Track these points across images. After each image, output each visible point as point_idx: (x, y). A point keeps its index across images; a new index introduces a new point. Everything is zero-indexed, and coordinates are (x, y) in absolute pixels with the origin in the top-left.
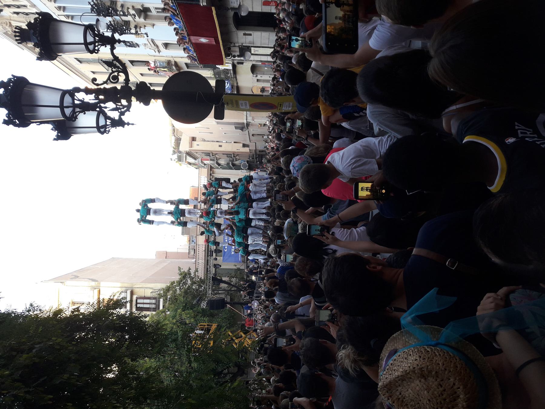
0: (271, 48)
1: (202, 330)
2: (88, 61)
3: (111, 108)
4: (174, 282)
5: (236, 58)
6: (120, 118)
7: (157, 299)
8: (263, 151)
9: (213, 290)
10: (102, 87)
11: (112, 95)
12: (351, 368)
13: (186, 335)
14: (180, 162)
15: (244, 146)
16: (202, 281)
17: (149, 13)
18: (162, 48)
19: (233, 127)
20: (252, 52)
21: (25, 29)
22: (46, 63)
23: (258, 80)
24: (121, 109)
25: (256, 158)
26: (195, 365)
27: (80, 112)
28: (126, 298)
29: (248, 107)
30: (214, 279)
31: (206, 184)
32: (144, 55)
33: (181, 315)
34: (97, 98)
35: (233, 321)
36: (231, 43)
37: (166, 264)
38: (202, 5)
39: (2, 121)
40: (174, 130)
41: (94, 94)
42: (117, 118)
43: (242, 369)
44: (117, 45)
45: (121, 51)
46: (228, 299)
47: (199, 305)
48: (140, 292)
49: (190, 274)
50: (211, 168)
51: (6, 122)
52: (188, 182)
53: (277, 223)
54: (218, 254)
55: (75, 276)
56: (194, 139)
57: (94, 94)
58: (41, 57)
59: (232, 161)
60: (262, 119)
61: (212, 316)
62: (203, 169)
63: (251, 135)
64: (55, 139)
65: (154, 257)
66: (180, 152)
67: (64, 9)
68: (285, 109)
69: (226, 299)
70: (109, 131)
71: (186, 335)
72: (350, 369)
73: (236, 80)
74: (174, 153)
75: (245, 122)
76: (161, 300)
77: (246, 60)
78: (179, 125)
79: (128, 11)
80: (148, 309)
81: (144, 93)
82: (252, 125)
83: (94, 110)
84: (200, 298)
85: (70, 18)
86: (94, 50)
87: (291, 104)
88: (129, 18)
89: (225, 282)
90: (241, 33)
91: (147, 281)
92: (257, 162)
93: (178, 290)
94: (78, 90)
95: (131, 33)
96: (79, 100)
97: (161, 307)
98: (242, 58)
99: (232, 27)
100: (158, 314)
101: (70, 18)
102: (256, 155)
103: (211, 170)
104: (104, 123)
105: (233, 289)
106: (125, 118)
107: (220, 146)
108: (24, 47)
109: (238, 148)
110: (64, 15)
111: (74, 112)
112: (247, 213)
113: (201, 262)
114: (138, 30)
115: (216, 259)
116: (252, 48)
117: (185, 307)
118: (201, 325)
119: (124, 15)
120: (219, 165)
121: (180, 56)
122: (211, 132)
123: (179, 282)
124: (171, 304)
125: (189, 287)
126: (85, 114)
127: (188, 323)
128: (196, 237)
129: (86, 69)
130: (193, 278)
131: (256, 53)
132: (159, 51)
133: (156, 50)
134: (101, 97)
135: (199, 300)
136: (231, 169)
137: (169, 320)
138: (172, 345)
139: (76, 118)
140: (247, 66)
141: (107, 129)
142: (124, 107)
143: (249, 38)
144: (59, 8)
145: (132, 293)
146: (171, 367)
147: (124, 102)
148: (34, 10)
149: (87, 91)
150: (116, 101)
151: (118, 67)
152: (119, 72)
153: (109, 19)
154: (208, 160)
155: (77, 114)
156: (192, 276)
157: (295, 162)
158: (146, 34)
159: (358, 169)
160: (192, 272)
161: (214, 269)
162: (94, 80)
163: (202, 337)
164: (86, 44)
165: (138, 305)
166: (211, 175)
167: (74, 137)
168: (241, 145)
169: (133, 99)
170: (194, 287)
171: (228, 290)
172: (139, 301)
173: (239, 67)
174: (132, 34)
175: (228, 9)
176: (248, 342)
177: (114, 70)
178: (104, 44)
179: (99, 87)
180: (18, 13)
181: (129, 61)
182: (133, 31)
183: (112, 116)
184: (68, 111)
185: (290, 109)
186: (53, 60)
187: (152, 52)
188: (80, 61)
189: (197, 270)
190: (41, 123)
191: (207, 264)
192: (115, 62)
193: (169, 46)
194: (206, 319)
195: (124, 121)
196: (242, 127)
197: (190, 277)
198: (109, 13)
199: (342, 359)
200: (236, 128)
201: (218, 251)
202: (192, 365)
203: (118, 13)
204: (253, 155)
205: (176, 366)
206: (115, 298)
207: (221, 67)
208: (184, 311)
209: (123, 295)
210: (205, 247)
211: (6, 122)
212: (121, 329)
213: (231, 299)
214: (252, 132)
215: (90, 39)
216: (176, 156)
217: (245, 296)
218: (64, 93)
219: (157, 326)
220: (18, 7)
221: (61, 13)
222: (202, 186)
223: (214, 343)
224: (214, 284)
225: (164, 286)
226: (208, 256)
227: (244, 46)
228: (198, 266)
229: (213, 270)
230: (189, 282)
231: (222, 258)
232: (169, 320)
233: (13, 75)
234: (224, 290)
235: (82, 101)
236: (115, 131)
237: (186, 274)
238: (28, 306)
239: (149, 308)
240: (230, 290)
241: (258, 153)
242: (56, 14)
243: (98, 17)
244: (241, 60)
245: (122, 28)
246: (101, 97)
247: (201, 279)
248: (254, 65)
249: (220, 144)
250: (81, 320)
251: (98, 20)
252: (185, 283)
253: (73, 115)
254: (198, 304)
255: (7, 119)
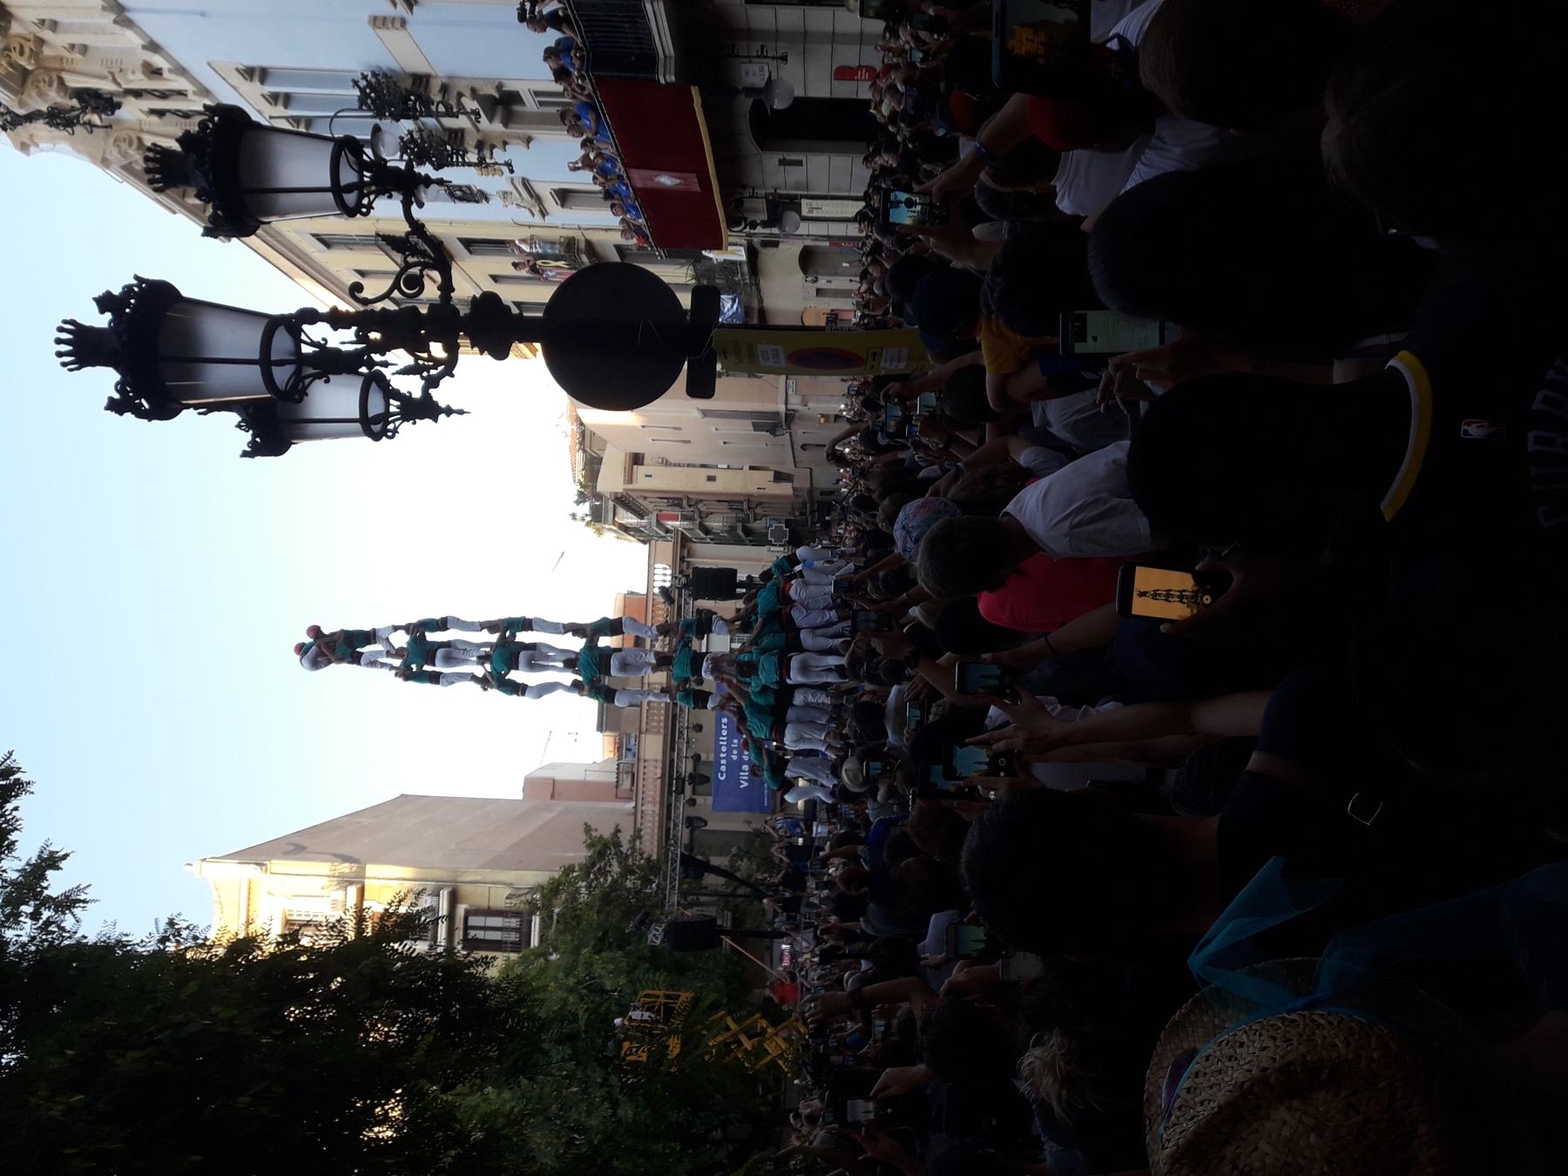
0: (856, 199)
1: (650, 1009)
2: (347, 243)
3: (401, 366)
4: (570, 869)
5: (759, 230)
6: (426, 396)
7: (524, 917)
9: (683, 894)
10: (378, 306)
11: (404, 328)
12: (1059, 1101)
15: (779, 477)
16: (652, 868)
17: (517, 108)
18: (551, 204)
19: (748, 423)
23: (819, 292)
24: (428, 369)
25: (812, 512)
26: (627, 1112)
28: (432, 910)
29: (783, 364)
32: (503, 224)
35: (741, 987)
36: (745, 187)
39: (105, 402)
40: (583, 434)
41: (354, 328)
42: (417, 394)
44: (426, 194)
45: (437, 214)
46: (725, 921)
47: (643, 936)
48: (476, 895)
49: (618, 845)
50: (684, 541)
51: (115, 406)
52: (614, 574)
54: (700, 788)
55: (296, 846)
56: (637, 459)
57: (354, 328)
60: (828, 399)
61: (679, 969)
62: (661, 543)
63: (797, 447)
64: (245, 454)
65: (518, 795)
66: (599, 497)
67: (287, 100)
68: (887, 366)
69: (719, 922)
70: (395, 431)
71: (600, 1023)
72: (1055, 1104)
73: (759, 290)
74: (582, 498)
75: (782, 408)
77: (787, 236)
78: (595, 417)
79: (459, 104)
81: (494, 328)
82: (803, 418)
83: (353, 371)
84: (647, 915)
86: (359, 205)
88: (462, 122)
89: (718, 871)
90: (772, 160)
91: (498, 863)
92: (813, 523)
94: (310, 316)
95: (465, 164)
96: (313, 344)
97: (535, 941)
98: (775, 231)
99: (748, 143)
100: (524, 960)
102: (812, 504)
103: (683, 546)
104: (381, 410)
106: (440, 395)
107: (711, 479)
108: (176, 207)
109: (759, 483)
110: (287, 118)
112: (784, 668)
113: (652, 809)
114: (487, 153)
115: (692, 802)
116: (804, 202)
117: (601, 940)
118: (646, 996)
119: (450, 113)
120: (707, 531)
121: (602, 225)
122: (670, 431)
123: (587, 869)
124: (563, 932)
125: (614, 881)
126: (327, 381)
127: (608, 987)
128: (638, 739)
129: (343, 264)
130: (627, 857)
131: (815, 214)
132: (544, 213)
133: (536, 210)
134: (375, 335)
135: (642, 922)
136: (740, 542)
137: (556, 979)
139: (303, 393)
140: (790, 251)
141: (391, 426)
142: (437, 362)
143: (796, 174)
144: (274, 98)
145: (454, 899)
146: (558, 1117)
150: (416, 345)
151: (423, 254)
152: (425, 266)
153: (407, 125)
154: (675, 518)
155: (307, 381)
157: (910, 513)
159: (1091, 527)
160: (625, 838)
161: (686, 832)
162: (356, 288)
163: (644, 1032)
164: (337, 189)
165: (472, 933)
166: (682, 559)
167: (300, 450)
168: (770, 475)
169: (464, 342)
170: (629, 884)
171: (725, 895)
172: (473, 921)
173: (767, 255)
174: (470, 164)
176: (776, 1045)
177: (410, 259)
178: (384, 189)
179: (370, 307)
180: (161, 113)
181: (462, 240)
182: (472, 157)
184: (282, 375)
185: (902, 365)
186: (249, 235)
187: (523, 216)
189: (637, 835)
190: (211, 408)
192: (414, 239)
194: (661, 977)
195: (436, 404)
196: (771, 424)
197: (619, 854)
200: (756, 427)
201: (699, 780)
202: (621, 1112)
204: (804, 504)
206: (402, 910)
208: (598, 952)
209: (426, 902)
210: (663, 769)
211: (115, 406)
213: (736, 921)
214: (801, 438)
215: (348, 176)
216: (585, 508)
217: (776, 914)
218: (273, 324)
219: (518, 989)
220: (164, 95)
221: (279, 110)
222: (656, 591)
223: (684, 1045)
226: (670, 793)
227: (781, 196)
228: (640, 820)
229: (684, 834)
230: (616, 868)
231: (710, 799)
232: (556, 979)
233: (136, 277)
234: (715, 893)
235: (321, 346)
236: (412, 432)
237: (606, 846)
238: (163, 925)
240: (733, 894)
241: (817, 497)
242: (260, 112)
244: (772, 235)
245: (445, 148)
246: (375, 335)
247: (649, 859)
248: (809, 250)
249: (711, 472)
250: (304, 968)
251: (377, 130)
252: (603, 872)
253: (295, 385)
255: (117, 396)
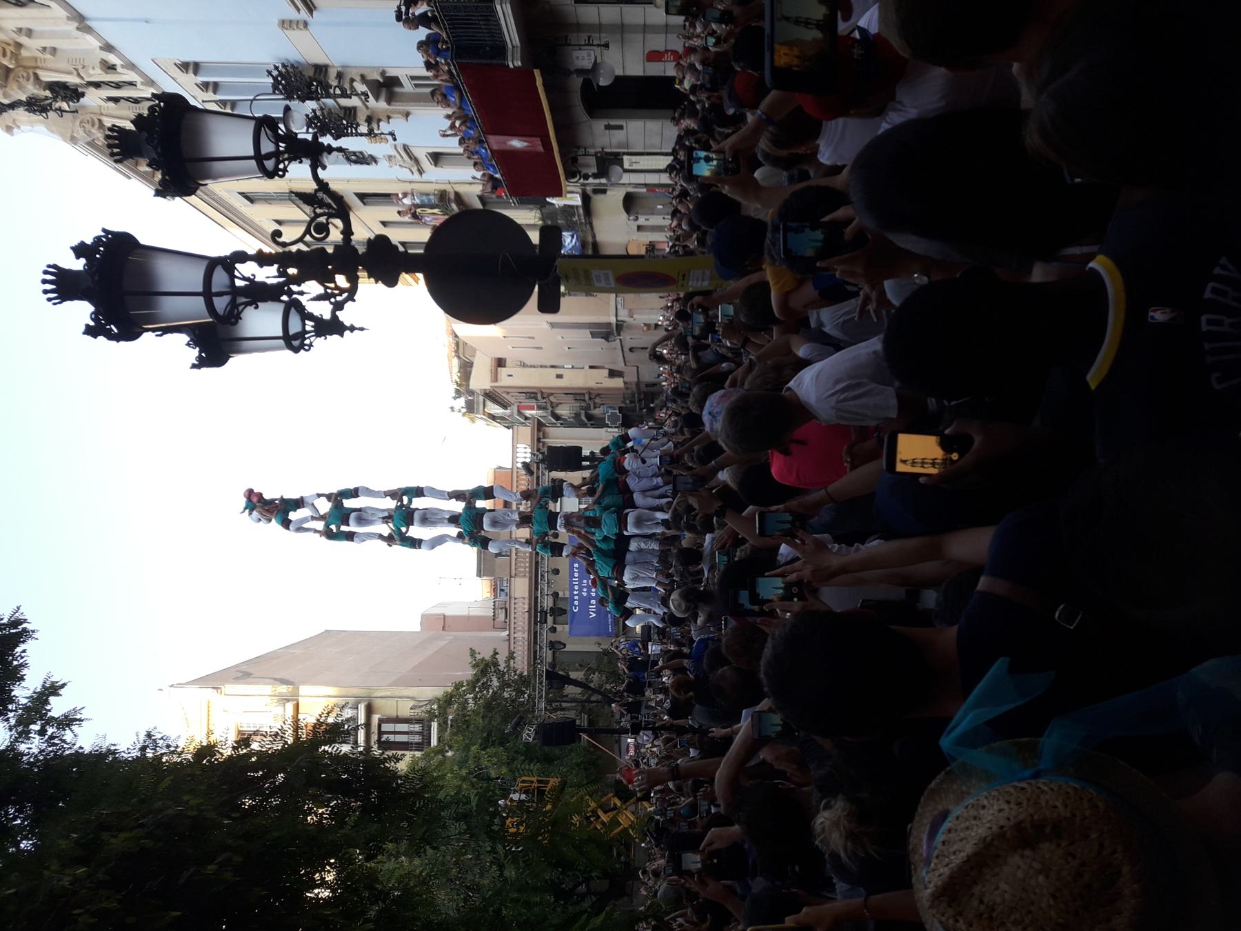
2: (267, 199)
3: (314, 295)
5: (591, 180)
7: (425, 723)
8: (654, 385)
9: (549, 701)
10: (294, 248)
11: (315, 265)
13: (488, 800)
14: (472, 415)
15: (613, 374)
16: (524, 681)
17: (398, 90)
18: (426, 164)
19: (587, 332)
20: (626, 166)
21: (130, 131)
22: (177, 204)
23: (639, 228)
24: (334, 296)
25: (640, 400)
26: (510, 873)
27: (247, 304)
29: (613, 284)
30: (551, 675)
31: (528, 460)
32: (389, 181)
33: (477, 758)
34: (282, 273)
35: (597, 770)
36: (579, 148)
37: (443, 643)
38: (511, 66)
40: (457, 344)
41: (276, 266)
43: (621, 881)
44: (327, 159)
45: (338, 174)
46: (583, 721)
47: (519, 735)
48: (387, 708)
49: (496, 664)
51: (91, 331)
52: (490, 453)
53: (687, 539)
54: (560, 618)
55: (243, 673)
56: (500, 363)
57: (276, 266)
58: (164, 190)
59: (587, 409)
60: (650, 311)
61: (548, 760)
62: (521, 428)
63: (626, 350)
64: (194, 366)
66: (472, 393)
67: (216, 87)
68: (694, 284)
70: (311, 345)
71: (488, 800)
72: (842, 855)
73: (592, 228)
74: (458, 394)
75: (613, 320)
76: (435, 725)
77: (613, 185)
78: (470, 331)
79: (352, 87)
80: (405, 746)
81: (385, 262)
82: (630, 327)
84: (521, 718)
85: (229, 106)
86: (276, 169)
87: (708, 272)
88: (354, 102)
89: (575, 683)
90: (599, 125)
91: (403, 681)
92: (641, 409)
93: (471, 701)
94: (241, 257)
95: (358, 134)
96: (244, 279)
98: (603, 181)
99: (580, 112)
100: (426, 756)
101: (229, 106)
102: (639, 394)
103: (539, 430)
105: (593, 698)
106: (345, 316)
107: (559, 376)
109: (598, 380)
110: (215, 102)
111: (233, 305)
112: (622, 522)
113: (522, 636)
114: (375, 126)
115: (553, 630)
116: (625, 157)
117: (486, 740)
118: (523, 782)
119: (344, 95)
120: (557, 417)
121: (465, 179)
122: (534, 342)
123: (473, 684)
124: (456, 734)
125: (495, 693)
126: (257, 307)
128: (509, 581)
129: (265, 216)
130: (504, 674)
131: (635, 167)
132: (421, 172)
133: (415, 169)
134: (292, 271)
135: (517, 724)
136: (585, 426)
137: (452, 771)
138: (456, 828)
140: (615, 196)
141: (307, 342)
142: (342, 291)
143: (618, 136)
144: (205, 86)
145: (370, 710)
147: (341, 281)
148: (147, 92)
149: (262, 259)
151: (329, 206)
152: (330, 216)
153: (311, 105)
156: (501, 668)
158: (392, 134)
160: (502, 659)
161: (550, 653)
162: (277, 234)
164: (259, 157)
165: (384, 738)
166: (539, 440)
167: (236, 361)
168: (606, 372)
169: (362, 274)
170: (506, 695)
172: (385, 727)
173: (598, 200)
174: (361, 135)
175: (568, 73)
177: (318, 211)
179: (287, 249)
180: (116, 100)
181: (357, 194)
182: (363, 129)
183: (316, 313)
184: (221, 304)
187: (405, 174)
188: (250, 198)
189: (511, 656)
191: (535, 643)
192: (320, 194)
193: (443, 160)
194: (535, 767)
196: (606, 332)
197: (498, 672)
198: (312, 93)
199: (823, 830)
200: (593, 335)
202: (507, 873)
203: (332, 91)
204: (633, 394)
205: (470, 877)
206: (330, 720)
207: (556, 202)
208: (484, 749)
209: (348, 713)
210: (530, 604)
211: (91, 331)
212: (344, 789)
213: (590, 722)
215: (267, 147)
216: (461, 402)
217: (622, 715)
218: (213, 263)
219: (423, 779)
220: (118, 86)
221: (210, 95)
222: (520, 465)
224: (550, 686)
225: (437, 692)
226: (536, 624)
227: (607, 153)
228: (513, 645)
229: (547, 655)
231: (567, 627)
232: (452, 771)
233: (104, 230)
235: (251, 281)
236: (323, 346)
237: (487, 665)
238: (142, 737)
239: (407, 743)
242: (197, 98)
243: (287, 102)
244: (601, 184)
245: (342, 122)
246: (292, 271)
247: (521, 675)
248: (631, 192)
249: (559, 371)
251: (287, 109)
252: (486, 686)
253: (231, 312)
254: (517, 732)
255: (92, 323)
